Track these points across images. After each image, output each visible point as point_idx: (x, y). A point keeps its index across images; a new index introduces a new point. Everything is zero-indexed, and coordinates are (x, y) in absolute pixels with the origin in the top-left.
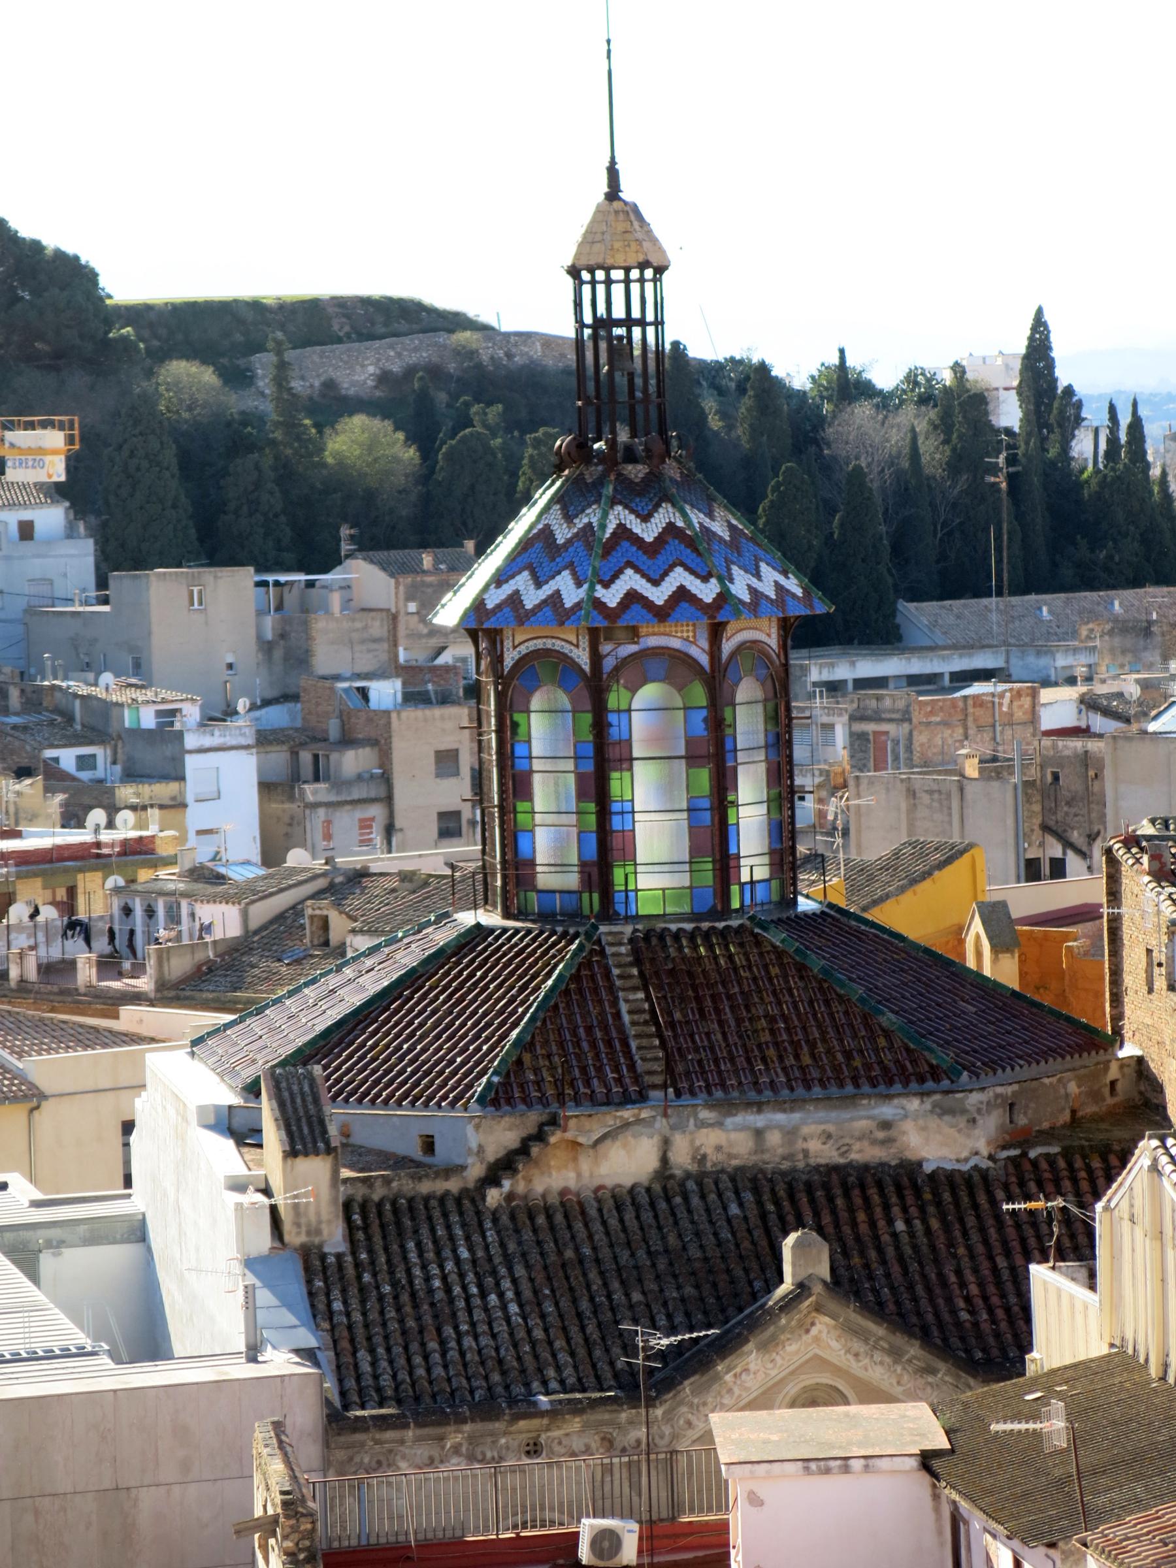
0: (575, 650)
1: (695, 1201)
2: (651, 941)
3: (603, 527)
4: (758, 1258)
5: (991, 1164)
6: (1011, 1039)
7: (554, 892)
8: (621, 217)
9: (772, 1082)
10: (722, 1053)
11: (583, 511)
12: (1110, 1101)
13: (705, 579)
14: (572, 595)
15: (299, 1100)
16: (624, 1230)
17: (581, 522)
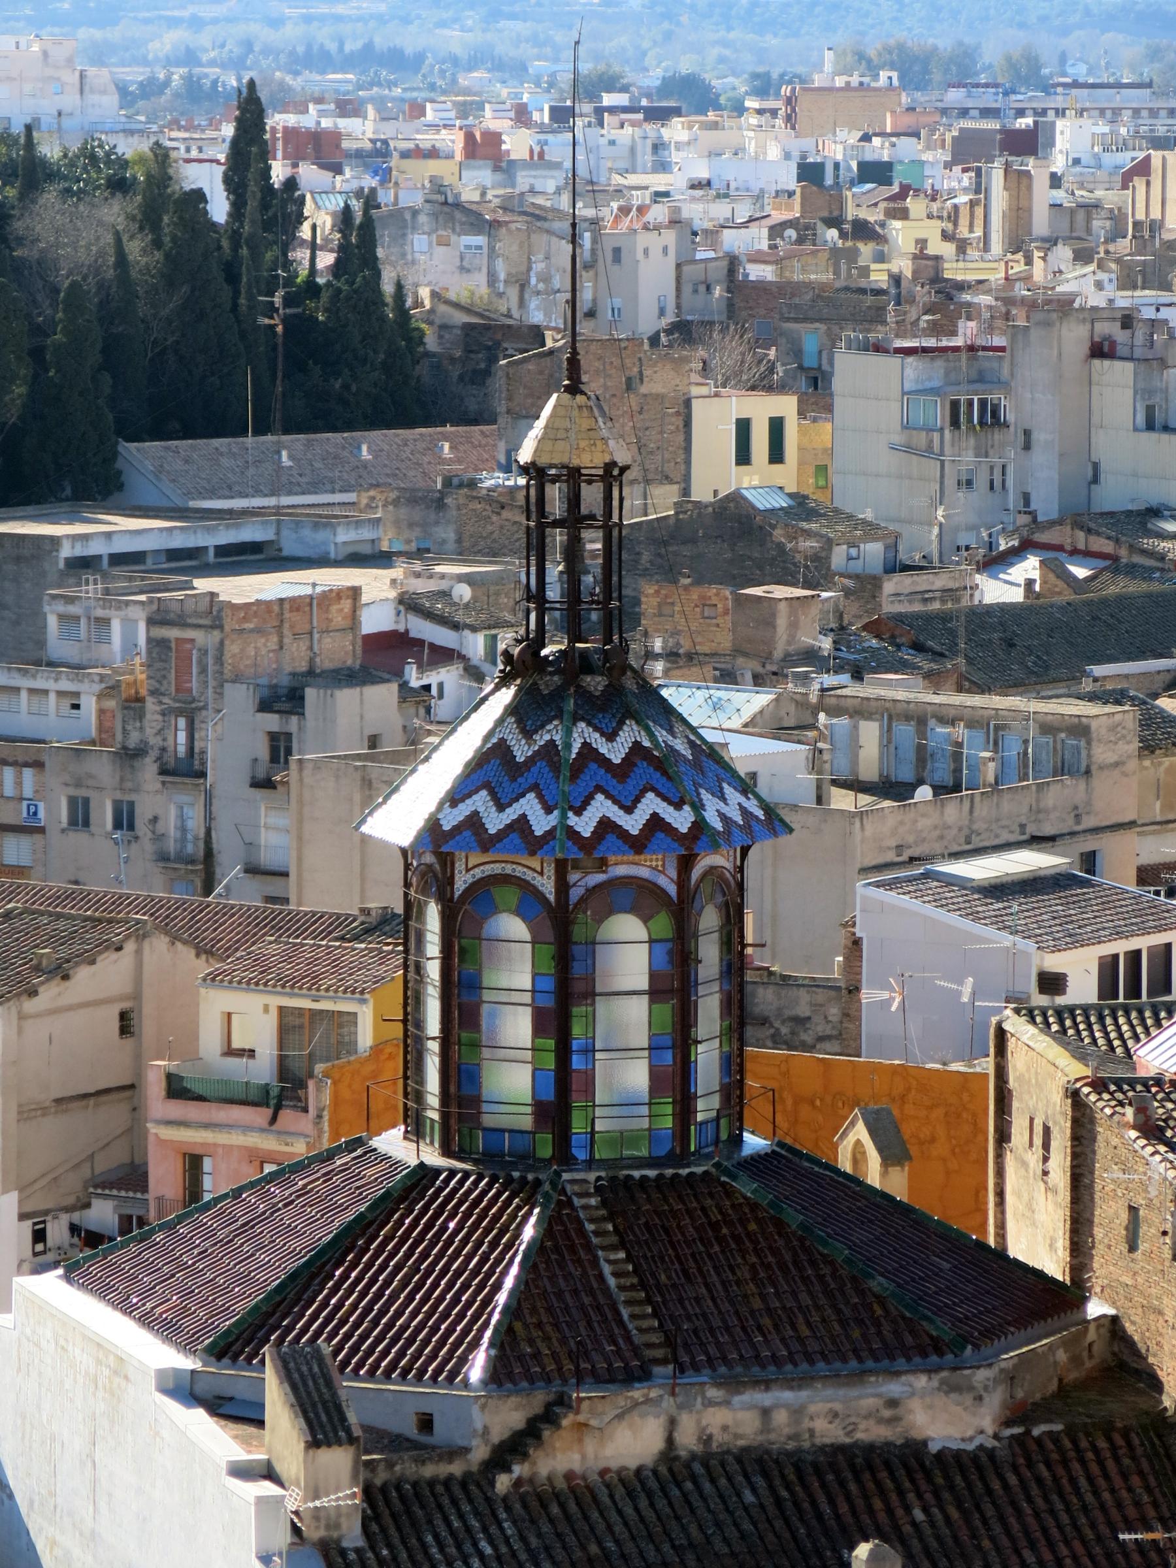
0: (539, 878)
1: (707, 1487)
2: (618, 1193)
3: (568, 746)
4: (785, 1552)
5: (996, 1444)
7: (503, 1131)
8: (585, 412)
9: (773, 1355)
10: (717, 1322)
11: (542, 726)
12: (1088, 1364)
13: (678, 806)
14: (541, 823)
15: (311, 1383)
16: (642, 1519)
17: (542, 738)
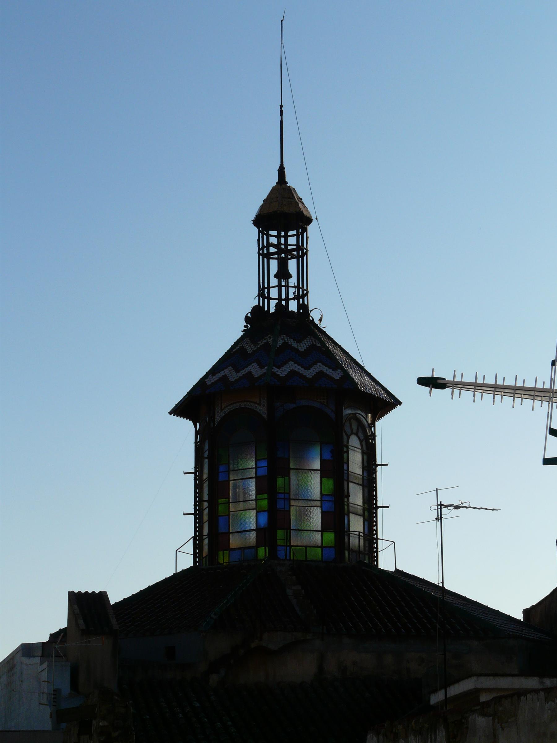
17: (261, 343)
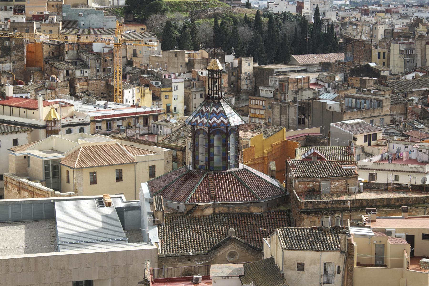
6: (269, 192)
13: (226, 119)
14: (205, 121)
17: (207, 109)
